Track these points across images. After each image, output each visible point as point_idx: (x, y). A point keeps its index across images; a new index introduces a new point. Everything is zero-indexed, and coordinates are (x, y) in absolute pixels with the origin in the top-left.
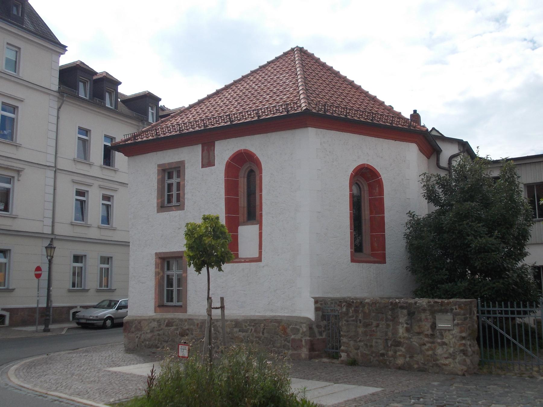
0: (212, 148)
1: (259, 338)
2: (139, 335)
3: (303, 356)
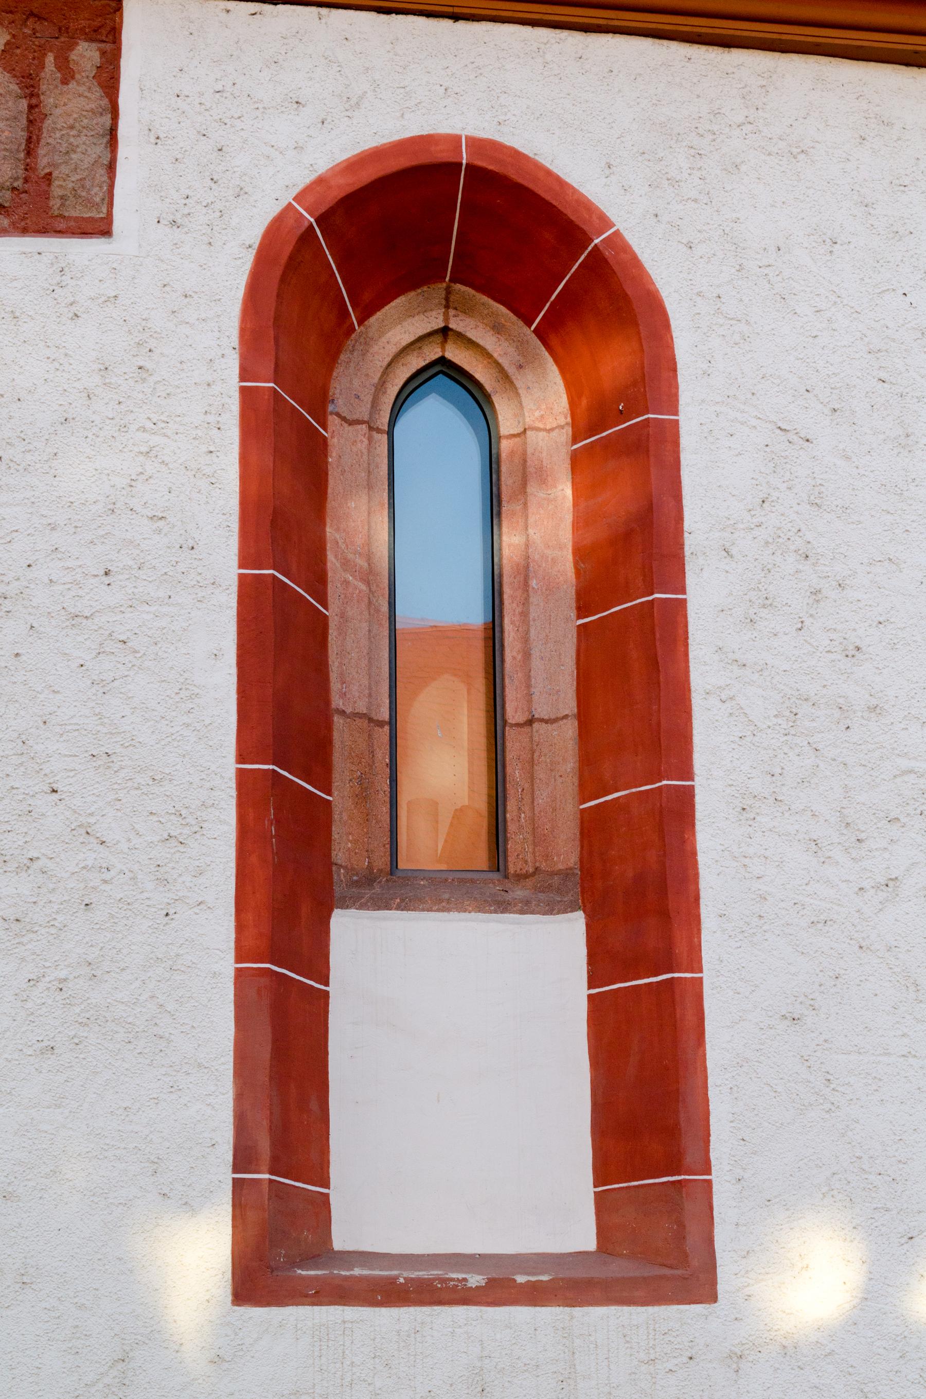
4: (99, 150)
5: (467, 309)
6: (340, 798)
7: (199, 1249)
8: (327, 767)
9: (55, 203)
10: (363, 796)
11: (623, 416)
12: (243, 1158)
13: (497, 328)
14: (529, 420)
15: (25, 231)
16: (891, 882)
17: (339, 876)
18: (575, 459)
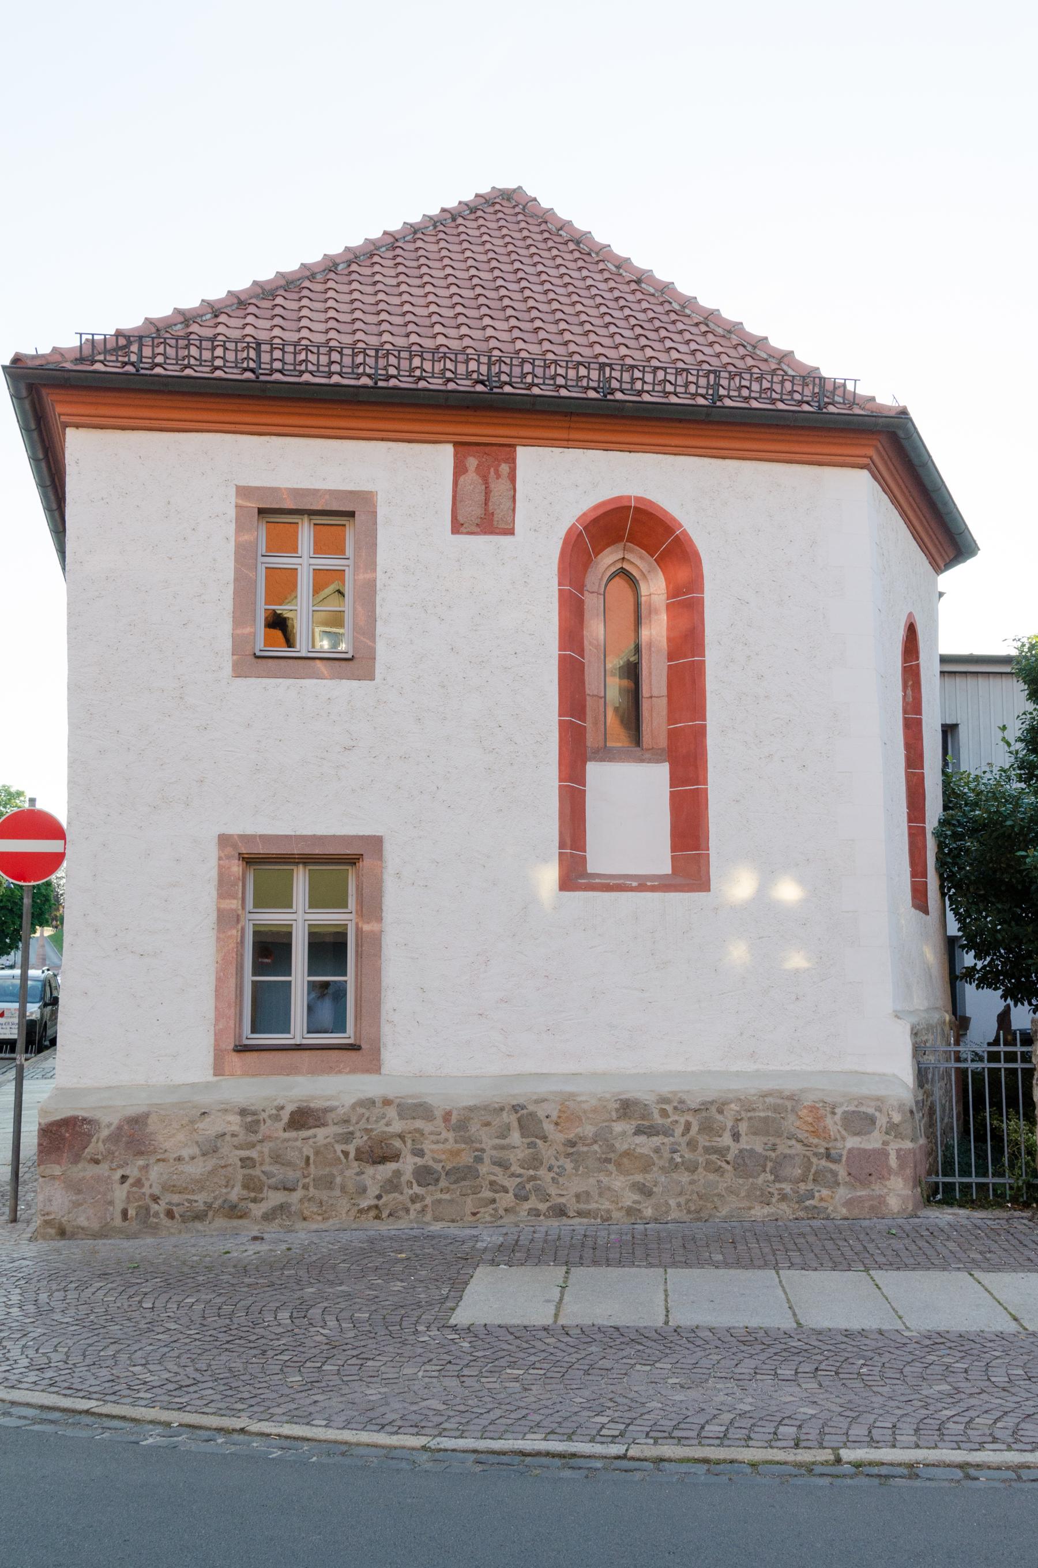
0: (504, 468)
1: (722, 1152)
2: (133, 1172)
3: (894, 1203)
4: (510, 504)
5: (631, 551)
6: (589, 724)
7: (549, 875)
8: (585, 714)
9: (495, 523)
10: (595, 724)
11: (685, 594)
12: (562, 845)
13: (641, 558)
14: (652, 591)
15: (485, 533)
16: (770, 756)
17: (589, 750)
18: (668, 606)
